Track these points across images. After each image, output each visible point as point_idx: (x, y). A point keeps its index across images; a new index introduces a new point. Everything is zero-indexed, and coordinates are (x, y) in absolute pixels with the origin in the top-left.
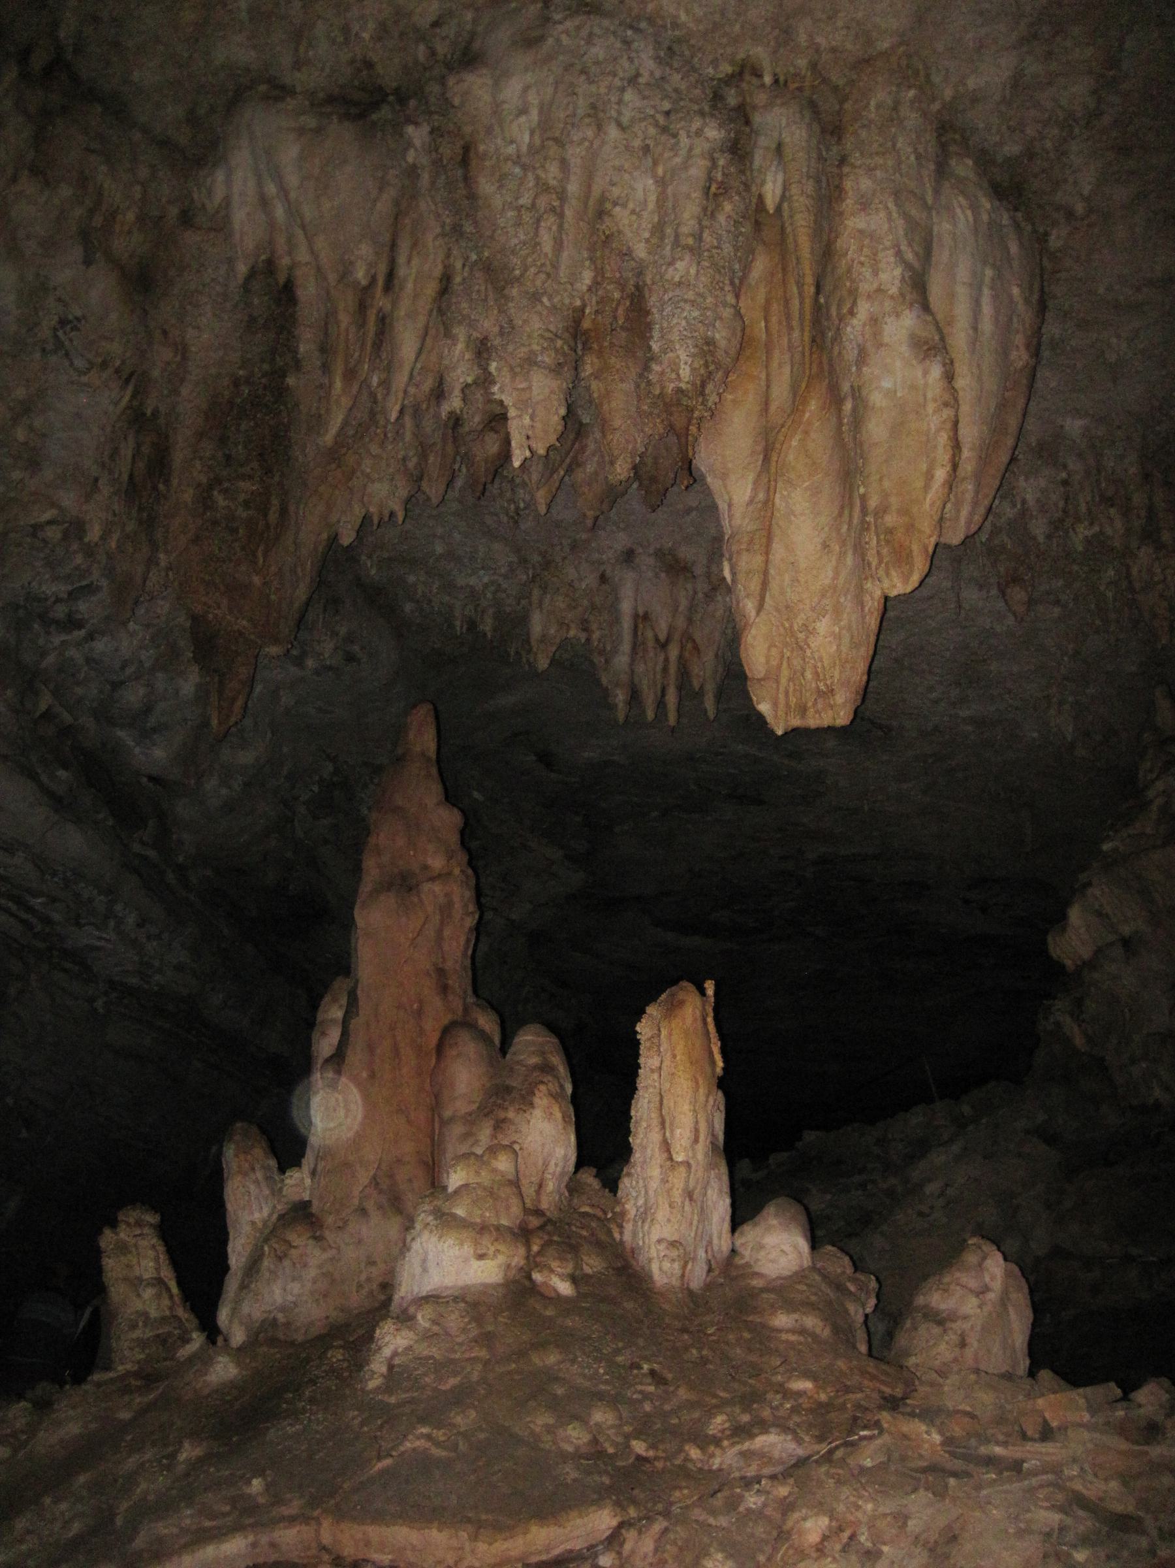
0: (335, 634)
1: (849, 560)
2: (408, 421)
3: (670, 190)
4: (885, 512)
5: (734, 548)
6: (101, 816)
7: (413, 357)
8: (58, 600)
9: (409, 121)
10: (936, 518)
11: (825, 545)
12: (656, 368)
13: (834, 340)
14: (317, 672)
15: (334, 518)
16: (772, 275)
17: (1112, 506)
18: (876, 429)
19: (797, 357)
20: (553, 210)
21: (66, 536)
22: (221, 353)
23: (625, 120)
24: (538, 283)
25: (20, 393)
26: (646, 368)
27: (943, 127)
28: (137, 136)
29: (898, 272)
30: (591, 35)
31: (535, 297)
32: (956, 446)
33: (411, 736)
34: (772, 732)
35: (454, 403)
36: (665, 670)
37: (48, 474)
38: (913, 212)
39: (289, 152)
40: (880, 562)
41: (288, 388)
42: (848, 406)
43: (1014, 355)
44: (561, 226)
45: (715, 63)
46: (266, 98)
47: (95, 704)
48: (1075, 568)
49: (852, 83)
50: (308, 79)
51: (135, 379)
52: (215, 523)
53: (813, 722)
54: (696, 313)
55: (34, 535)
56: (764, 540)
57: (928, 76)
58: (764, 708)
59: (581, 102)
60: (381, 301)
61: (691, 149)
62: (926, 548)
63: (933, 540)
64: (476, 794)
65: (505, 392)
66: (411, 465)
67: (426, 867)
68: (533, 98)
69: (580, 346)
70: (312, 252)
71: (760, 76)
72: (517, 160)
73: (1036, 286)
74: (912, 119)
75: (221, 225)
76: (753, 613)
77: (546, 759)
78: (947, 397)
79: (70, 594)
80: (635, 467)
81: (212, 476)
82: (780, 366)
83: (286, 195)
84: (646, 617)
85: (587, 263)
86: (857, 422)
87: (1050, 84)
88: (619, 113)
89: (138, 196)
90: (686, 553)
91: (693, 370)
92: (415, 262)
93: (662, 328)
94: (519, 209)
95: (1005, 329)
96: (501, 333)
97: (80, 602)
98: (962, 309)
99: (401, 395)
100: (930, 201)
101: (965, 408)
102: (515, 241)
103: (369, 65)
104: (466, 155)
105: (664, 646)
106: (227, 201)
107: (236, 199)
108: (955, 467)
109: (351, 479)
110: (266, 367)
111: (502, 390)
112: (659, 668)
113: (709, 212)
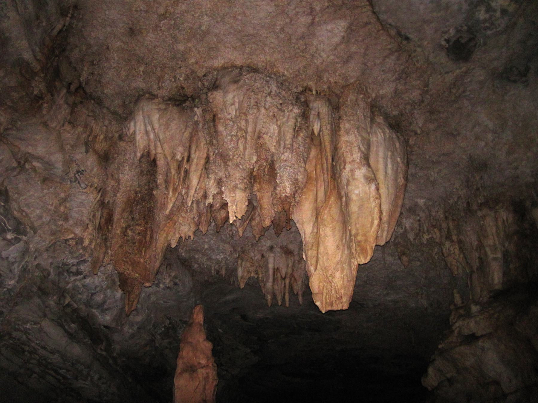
0: (170, 276)
1: (346, 252)
2: (195, 205)
3: (282, 129)
4: (357, 235)
5: (306, 249)
6: (86, 340)
7: (196, 185)
8: (73, 265)
9: (195, 106)
10: (375, 237)
11: (338, 247)
12: (278, 189)
13: (338, 177)
14: (164, 289)
15: (169, 238)
16: (317, 156)
17: (435, 228)
18: (354, 207)
19: (326, 184)
20: (243, 136)
21: (77, 244)
22: (131, 183)
23: (267, 106)
24: (238, 161)
25: (63, 195)
26: (275, 189)
27: (372, 106)
28: (105, 111)
29: (359, 154)
30: (255, 79)
31: (237, 165)
32: (381, 212)
33: (195, 316)
34: (321, 312)
35: (210, 200)
36: (285, 287)
37: (71, 222)
38: (363, 135)
39: (156, 117)
40: (357, 252)
41: (154, 195)
42: (344, 199)
43: (399, 180)
44: (246, 142)
45: (296, 87)
46: (148, 99)
47: (85, 301)
48: (424, 249)
49: (342, 93)
50: (163, 93)
51: (101, 191)
52: (128, 241)
53: (335, 308)
54: (291, 170)
55: (65, 243)
56: (316, 246)
57: (367, 90)
58: (318, 304)
59: (252, 101)
60: (185, 166)
61: (289, 116)
62: (372, 247)
63: (374, 245)
64: (220, 330)
65: (227, 197)
66: (196, 220)
67: (199, 363)
68: (236, 100)
69: (253, 181)
70: (162, 149)
71: (312, 91)
72: (231, 120)
73: (406, 157)
74: (362, 104)
75: (132, 140)
76: (313, 271)
77: (244, 317)
78: (377, 196)
79: (77, 263)
80: (272, 221)
81: (127, 224)
82: (321, 186)
83: (154, 130)
84: (278, 269)
85: (255, 154)
86: (347, 205)
87: (407, 92)
88: (265, 104)
89: (105, 130)
90: (291, 247)
91: (290, 189)
92: (197, 153)
93: (280, 175)
94: (232, 136)
95: (396, 172)
96: (226, 177)
97: (81, 266)
98: (381, 166)
99: (192, 197)
100: (369, 130)
101: (383, 199)
102: (230, 146)
103: (183, 88)
104: (214, 118)
105: (284, 279)
106: (135, 132)
107: (137, 132)
108: (381, 219)
109: (175, 225)
110: (146, 187)
111: (226, 197)
112: (283, 285)
113: (295, 137)
